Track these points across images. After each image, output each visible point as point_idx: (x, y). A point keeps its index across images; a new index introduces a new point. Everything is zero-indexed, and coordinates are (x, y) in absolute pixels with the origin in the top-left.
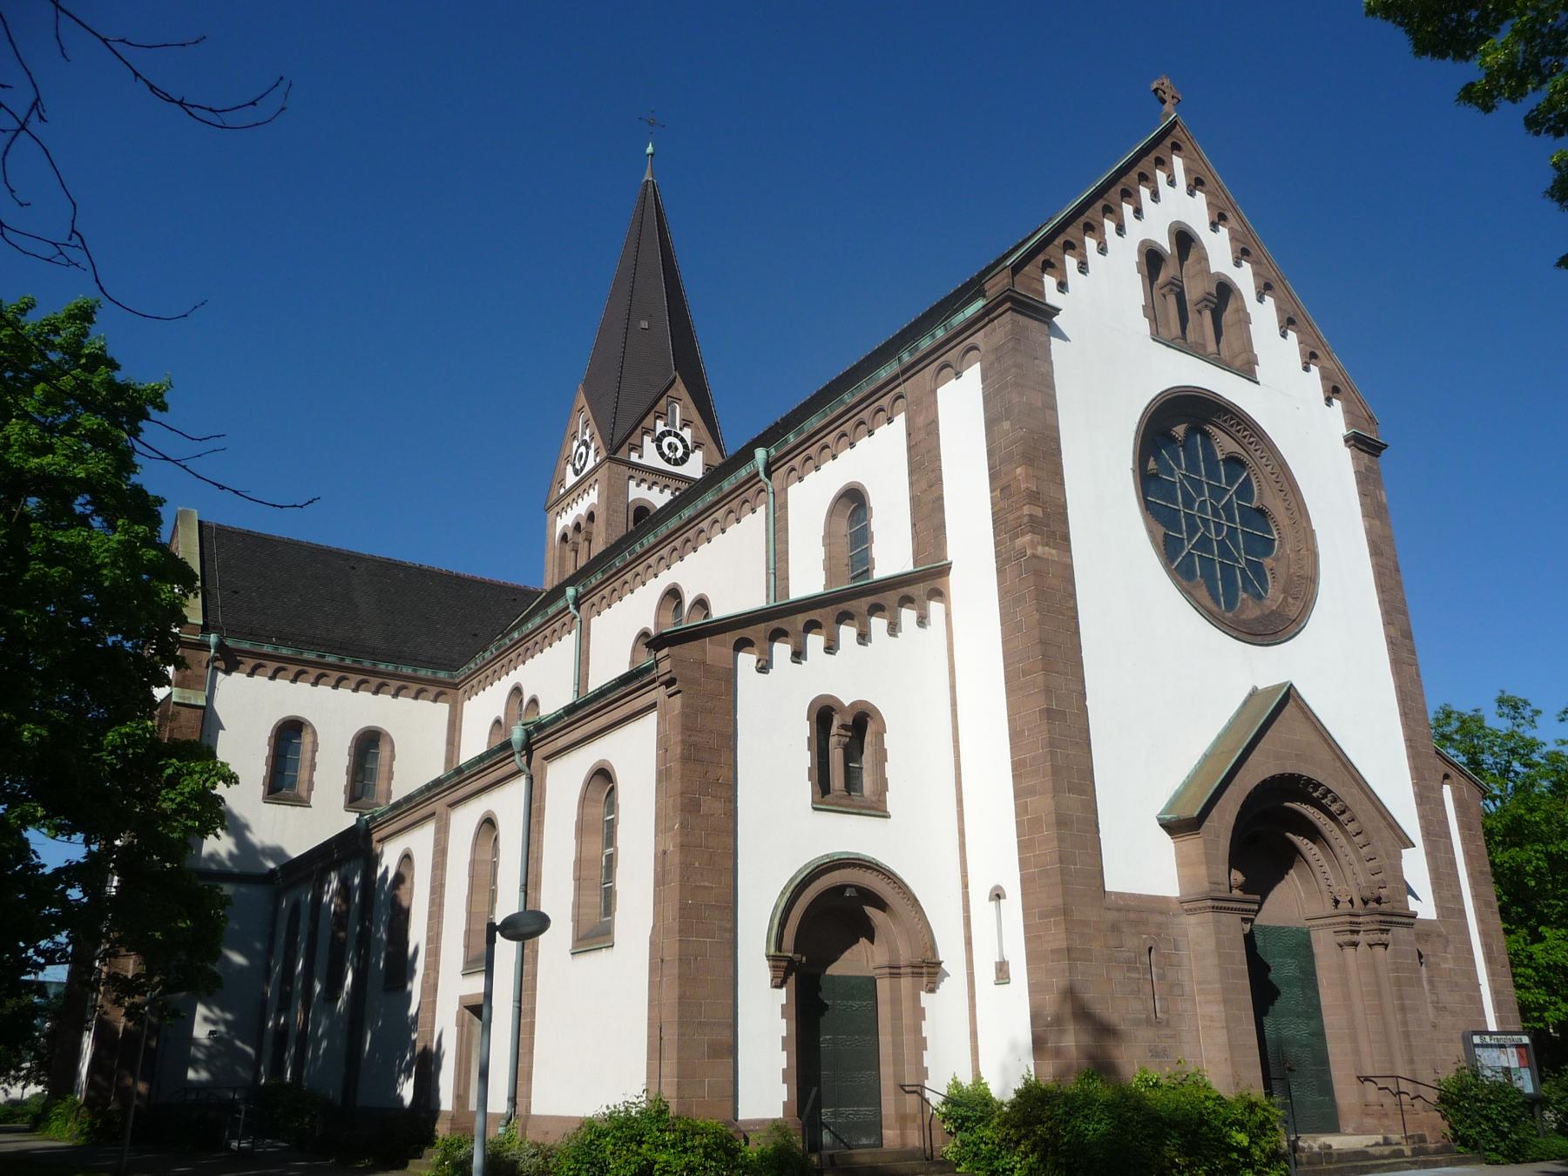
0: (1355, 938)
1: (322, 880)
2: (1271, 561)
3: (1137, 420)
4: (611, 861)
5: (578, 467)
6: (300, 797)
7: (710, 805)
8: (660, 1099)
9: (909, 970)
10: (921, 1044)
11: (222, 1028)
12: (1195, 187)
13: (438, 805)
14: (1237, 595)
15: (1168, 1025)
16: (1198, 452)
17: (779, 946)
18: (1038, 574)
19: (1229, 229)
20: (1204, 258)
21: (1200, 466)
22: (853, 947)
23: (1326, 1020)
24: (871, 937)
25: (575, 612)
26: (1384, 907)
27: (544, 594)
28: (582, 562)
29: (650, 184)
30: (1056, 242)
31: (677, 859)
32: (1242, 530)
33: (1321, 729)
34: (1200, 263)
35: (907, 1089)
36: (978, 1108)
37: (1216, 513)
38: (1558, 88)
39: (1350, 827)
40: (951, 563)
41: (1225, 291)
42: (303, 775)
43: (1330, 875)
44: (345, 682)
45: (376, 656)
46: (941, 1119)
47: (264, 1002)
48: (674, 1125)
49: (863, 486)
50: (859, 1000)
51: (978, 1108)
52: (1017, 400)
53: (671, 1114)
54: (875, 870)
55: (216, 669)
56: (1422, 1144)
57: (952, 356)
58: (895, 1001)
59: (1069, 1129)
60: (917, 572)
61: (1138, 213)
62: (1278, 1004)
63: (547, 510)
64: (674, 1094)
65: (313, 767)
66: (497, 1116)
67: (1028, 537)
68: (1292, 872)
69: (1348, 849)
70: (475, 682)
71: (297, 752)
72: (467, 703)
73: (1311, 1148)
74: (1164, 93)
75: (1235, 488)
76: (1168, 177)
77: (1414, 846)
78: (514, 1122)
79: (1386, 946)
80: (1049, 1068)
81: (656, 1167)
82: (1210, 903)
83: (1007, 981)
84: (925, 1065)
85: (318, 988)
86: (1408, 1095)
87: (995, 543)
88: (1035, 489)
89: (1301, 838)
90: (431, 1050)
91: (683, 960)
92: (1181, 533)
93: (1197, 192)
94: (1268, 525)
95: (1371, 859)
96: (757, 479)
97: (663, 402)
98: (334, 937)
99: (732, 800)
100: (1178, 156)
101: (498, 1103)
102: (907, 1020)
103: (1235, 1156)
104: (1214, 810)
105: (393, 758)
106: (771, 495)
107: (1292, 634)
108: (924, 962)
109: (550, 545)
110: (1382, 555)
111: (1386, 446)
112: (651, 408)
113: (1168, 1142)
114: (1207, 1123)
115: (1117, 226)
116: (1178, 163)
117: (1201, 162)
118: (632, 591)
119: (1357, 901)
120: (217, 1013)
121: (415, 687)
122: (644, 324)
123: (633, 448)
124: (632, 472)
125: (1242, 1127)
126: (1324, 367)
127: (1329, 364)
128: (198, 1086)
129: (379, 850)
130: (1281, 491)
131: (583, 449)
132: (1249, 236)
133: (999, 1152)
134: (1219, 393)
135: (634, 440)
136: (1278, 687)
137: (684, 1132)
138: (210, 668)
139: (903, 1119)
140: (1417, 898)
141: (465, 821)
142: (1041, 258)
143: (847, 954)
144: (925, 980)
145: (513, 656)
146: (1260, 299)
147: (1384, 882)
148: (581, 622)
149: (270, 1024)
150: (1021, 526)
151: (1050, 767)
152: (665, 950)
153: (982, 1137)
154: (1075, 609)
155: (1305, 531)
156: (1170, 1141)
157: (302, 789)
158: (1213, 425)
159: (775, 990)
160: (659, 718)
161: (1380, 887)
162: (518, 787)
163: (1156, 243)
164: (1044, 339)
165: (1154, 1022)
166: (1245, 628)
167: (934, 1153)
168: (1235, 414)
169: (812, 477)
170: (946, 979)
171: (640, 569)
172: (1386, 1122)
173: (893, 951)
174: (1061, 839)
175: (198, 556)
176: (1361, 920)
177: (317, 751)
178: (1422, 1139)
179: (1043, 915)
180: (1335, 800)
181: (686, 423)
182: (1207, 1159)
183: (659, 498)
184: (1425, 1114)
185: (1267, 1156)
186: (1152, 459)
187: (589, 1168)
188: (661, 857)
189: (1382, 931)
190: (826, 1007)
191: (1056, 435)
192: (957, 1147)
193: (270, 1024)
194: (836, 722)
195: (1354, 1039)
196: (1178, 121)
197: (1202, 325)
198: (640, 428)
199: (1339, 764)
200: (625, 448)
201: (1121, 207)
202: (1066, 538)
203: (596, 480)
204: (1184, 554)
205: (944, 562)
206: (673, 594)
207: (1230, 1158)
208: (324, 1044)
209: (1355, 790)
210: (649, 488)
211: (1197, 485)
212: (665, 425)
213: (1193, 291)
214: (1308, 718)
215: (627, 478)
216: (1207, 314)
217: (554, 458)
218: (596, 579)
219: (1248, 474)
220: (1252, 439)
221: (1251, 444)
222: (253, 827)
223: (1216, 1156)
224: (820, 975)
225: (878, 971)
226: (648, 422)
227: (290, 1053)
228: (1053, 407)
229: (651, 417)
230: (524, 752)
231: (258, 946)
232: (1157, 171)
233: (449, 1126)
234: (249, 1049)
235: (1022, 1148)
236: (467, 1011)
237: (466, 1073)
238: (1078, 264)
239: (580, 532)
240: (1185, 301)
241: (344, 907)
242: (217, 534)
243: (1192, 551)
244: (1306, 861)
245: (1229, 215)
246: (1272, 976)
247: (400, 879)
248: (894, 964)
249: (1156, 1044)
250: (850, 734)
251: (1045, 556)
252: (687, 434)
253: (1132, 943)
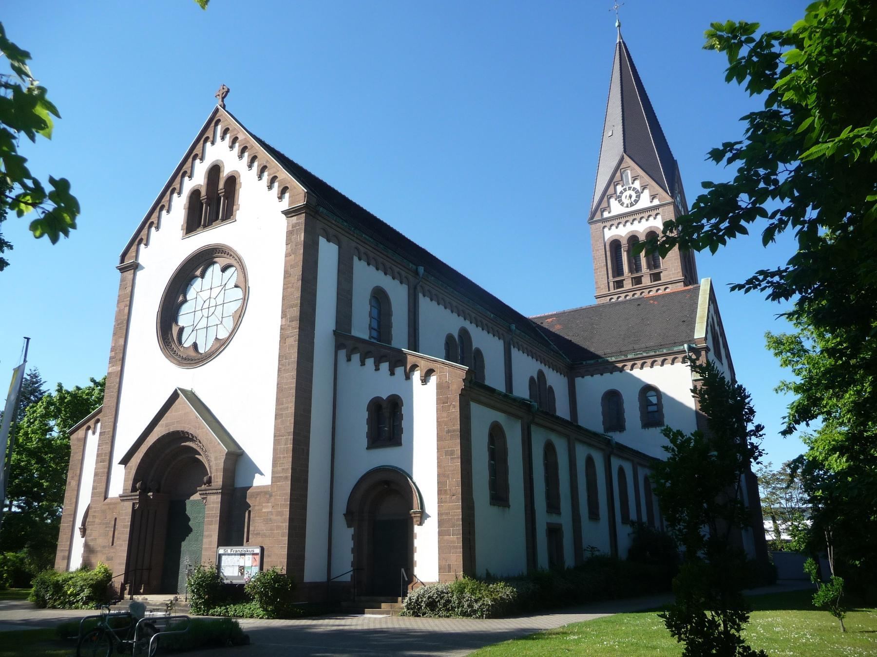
44: (655, 363)
181: (635, 179)
198: (606, 196)
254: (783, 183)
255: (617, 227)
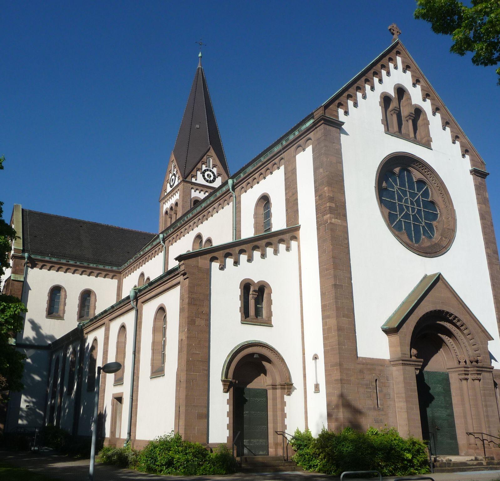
0: (466, 377)
1: (67, 348)
2: (436, 222)
3: (378, 167)
4: (165, 342)
5: (172, 184)
6: (60, 316)
7: (200, 322)
8: (178, 434)
9: (280, 387)
10: (284, 416)
11: (31, 404)
12: (406, 69)
13: (106, 320)
14: (421, 237)
15: (383, 410)
16: (405, 178)
17: (226, 376)
18: (332, 230)
19: (421, 86)
20: (410, 99)
21: (406, 184)
22: (258, 377)
23: (455, 410)
24: (265, 372)
25: (163, 244)
26: (479, 364)
27: (156, 236)
28: (173, 221)
29: (200, 69)
30: (344, 95)
31: (186, 343)
32: (423, 210)
33: (452, 291)
34: (407, 101)
35: (278, 433)
36: (305, 441)
37: (412, 203)
38: (479, 48)
39: (465, 332)
40: (300, 226)
41: (418, 111)
42: (61, 307)
43: (457, 351)
45: (89, 261)
46: (291, 445)
47: (47, 394)
48: (183, 444)
49: (268, 194)
50: (260, 398)
51: (305, 441)
52: (325, 160)
53: (182, 440)
54: (266, 347)
55: (28, 266)
56: (492, 461)
57: (301, 142)
58: (274, 399)
59: (337, 450)
60: (255, 237)
61: (381, 81)
62: (433, 403)
63: (160, 202)
64: (183, 432)
65: (65, 304)
66: (124, 440)
67: (328, 216)
68: (441, 349)
69: (465, 341)
70: (127, 271)
71: (59, 298)
72: (124, 279)
73: (442, 461)
74: (394, 30)
75: (421, 193)
76: (394, 65)
77: (494, 340)
78: (130, 442)
79: (480, 380)
80: (334, 425)
81: (175, 460)
82: (401, 362)
83: (319, 391)
84: (285, 424)
85: (65, 390)
86: (488, 441)
87: (316, 218)
88: (332, 196)
89: (445, 336)
90: (102, 414)
91: (188, 381)
92: (397, 212)
93: (407, 71)
94: (436, 208)
95: (474, 345)
96: (229, 192)
97: (205, 157)
98: (71, 370)
99: (209, 320)
100: (399, 56)
101: (124, 435)
102: (279, 406)
103: (406, 462)
104: (404, 325)
105: (96, 301)
106: (235, 198)
107: (443, 253)
108: (286, 383)
109: (161, 215)
110: (485, 219)
111: (489, 174)
112: (200, 160)
113: (377, 456)
114: (394, 449)
115: (371, 87)
116: (399, 59)
117: (409, 58)
118: (184, 236)
119: (468, 362)
120: (29, 399)
121: (104, 273)
122: (198, 126)
123: (193, 176)
124: (192, 186)
125: (409, 451)
126: (462, 142)
127: (464, 140)
128: (22, 426)
129: (86, 337)
130: (441, 194)
131: (173, 177)
132: (430, 88)
133: (312, 459)
134: (414, 154)
135: (193, 173)
136: (435, 275)
137: (186, 447)
138: (26, 266)
139: (276, 445)
140: (496, 361)
141: (115, 326)
142: (337, 102)
143: (256, 380)
144: (286, 391)
145: (141, 261)
146: (434, 114)
147: (480, 354)
148: (165, 248)
149: (49, 403)
150: (326, 211)
151: (335, 307)
152: (181, 377)
153: (306, 452)
154: (348, 244)
155: (451, 210)
156: (378, 456)
157: (61, 313)
158: (412, 167)
159: (224, 393)
160: (181, 287)
161: (478, 356)
162: (133, 314)
163: (388, 93)
164: (338, 135)
165: (377, 408)
166: (423, 250)
167: (288, 458)
168: (421, 163)
169: (250, 191)
170: (295, 390)
171: (187, 227)
172: (477, 451)
173: (274, 379)
174: (339, 336)
175: (21, 223)
176: (469, 369)
177: (66, 298)
178: (492, 458)
179: (332, 366)
180: (459, 321)
181: (214, 166)
182: (394, 463)
183: (202, 196)
184: (494, 448)
185: (420, 463)
186: (384, 182)
187: (151, 459)
188: (181, 341)
189: (478, 374)
190: (246, 400)
191: (342, 174)
192: (297, 456)
193: (49, 403)
194: (252, 289)
195: (465, 417)
196: (399, 42)
197: (408, 126)
199: (461, 306)
200: (190, 176)
201: (373, 79)
202: (345, 216)
203: (179, 190)
204: (397, 221)
205: (298, 225)
206: (199, 237)
207: (404, 464)
208: (67, 411)
209: (468, 316)
210: (200, 192)
211: (404, 193)
212: (206, 167)
213: (405, 112)
214: (448, 287)
215: (190, 188)
216: (410, 122)
217: (162, 181)
218: (171, 231)
219: (427, 187)
220: (428, 173)
221: (428, 174)
222: (43, 328)
223: (398, 462)
224: (244, 389)
225: (268, 387)
226: (199, 166)
227: (55, 414)
228: (341, 162)
229: (200, 164)
230: (135, 300)
231: (45, 373)
232: (390, 63)
233: (108, 443)
234: (42, 413)
235: (320, 457)
236: (115, 400)
237: (115, 423)
238: (354, 103)
239: (172, 210)
240: (401, 116)
241: (74, 359)
242: (29, 214)
243: (401, 219)
244: (447, 345)
245: (421, 80)
246: (431, 391)
247: (93, 348)
248: (273, 384)
249: (378, 418)
250: (257, 294)
251: (336, 223)
252: (215, 170)
253: (369, 377)
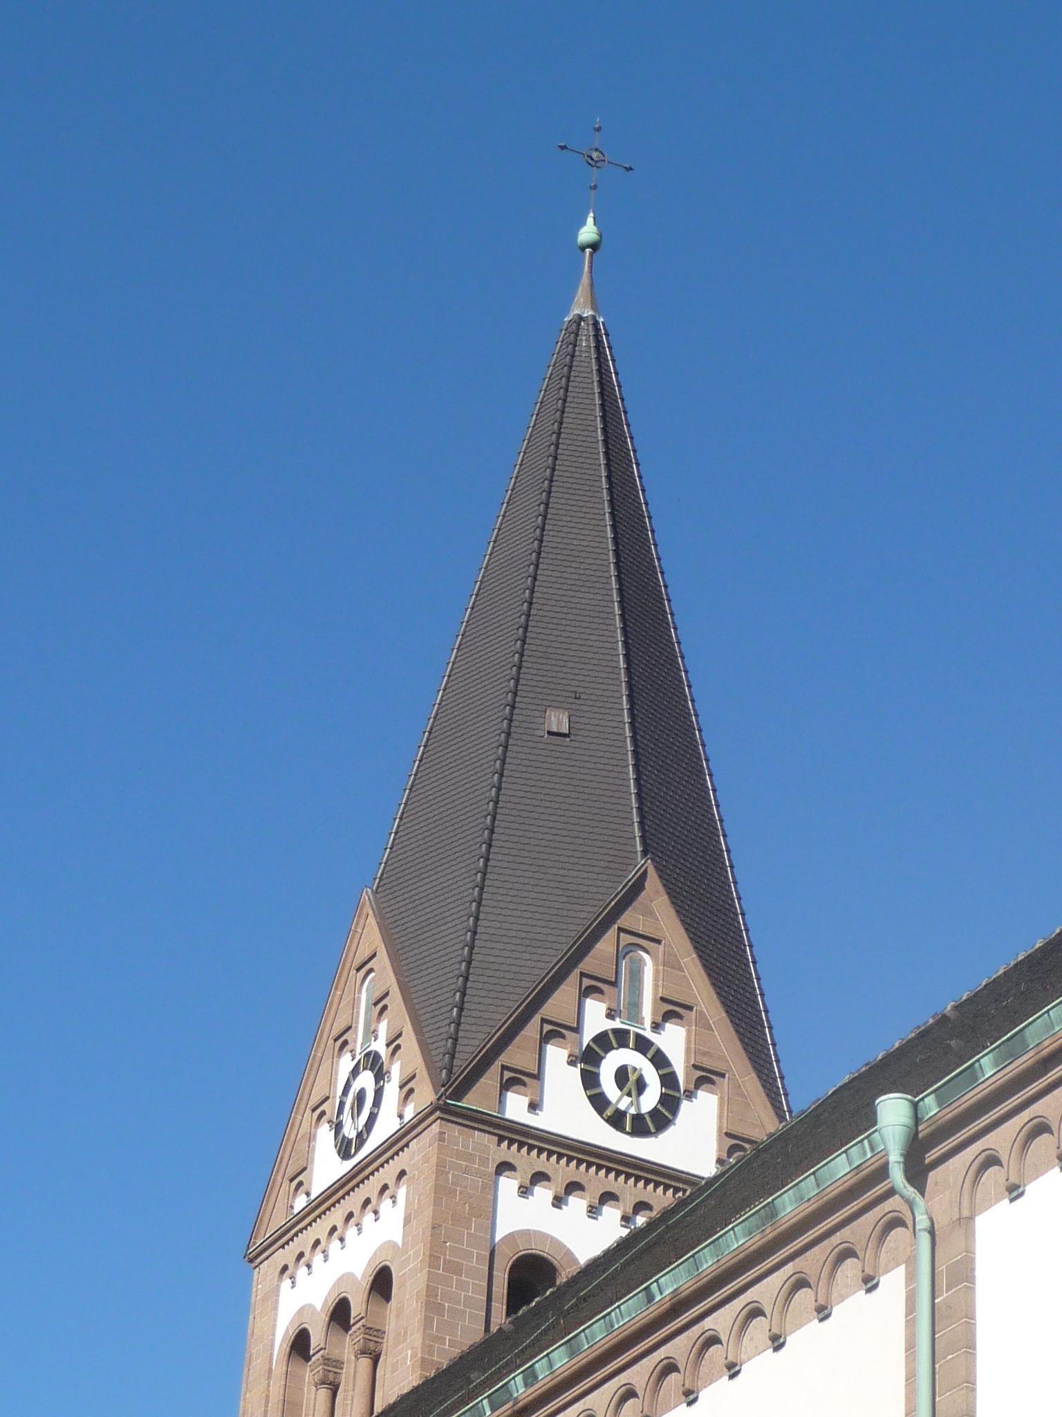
181: (671, 1011)
254: (403, 1399)
255: (558, 1202)
